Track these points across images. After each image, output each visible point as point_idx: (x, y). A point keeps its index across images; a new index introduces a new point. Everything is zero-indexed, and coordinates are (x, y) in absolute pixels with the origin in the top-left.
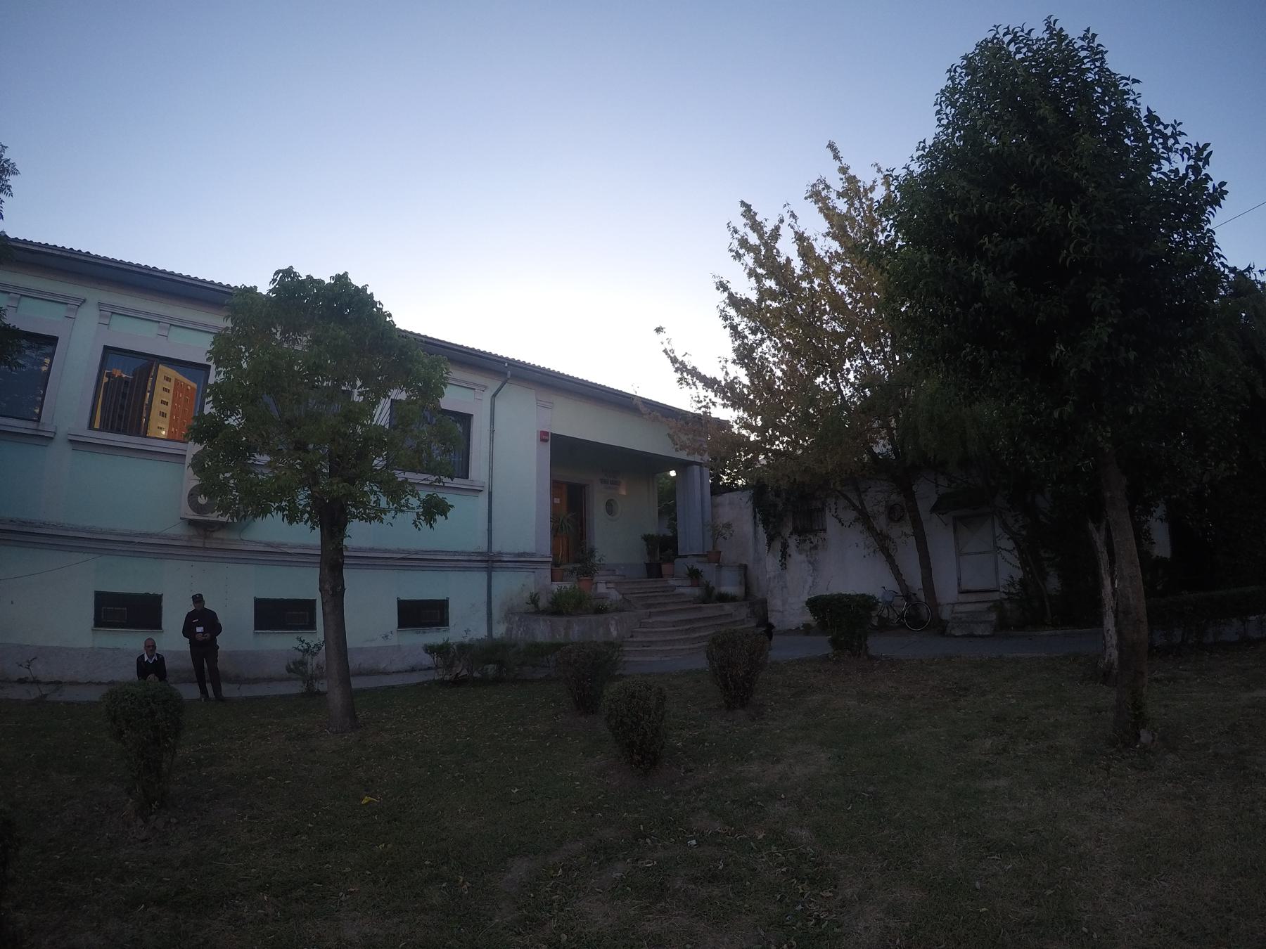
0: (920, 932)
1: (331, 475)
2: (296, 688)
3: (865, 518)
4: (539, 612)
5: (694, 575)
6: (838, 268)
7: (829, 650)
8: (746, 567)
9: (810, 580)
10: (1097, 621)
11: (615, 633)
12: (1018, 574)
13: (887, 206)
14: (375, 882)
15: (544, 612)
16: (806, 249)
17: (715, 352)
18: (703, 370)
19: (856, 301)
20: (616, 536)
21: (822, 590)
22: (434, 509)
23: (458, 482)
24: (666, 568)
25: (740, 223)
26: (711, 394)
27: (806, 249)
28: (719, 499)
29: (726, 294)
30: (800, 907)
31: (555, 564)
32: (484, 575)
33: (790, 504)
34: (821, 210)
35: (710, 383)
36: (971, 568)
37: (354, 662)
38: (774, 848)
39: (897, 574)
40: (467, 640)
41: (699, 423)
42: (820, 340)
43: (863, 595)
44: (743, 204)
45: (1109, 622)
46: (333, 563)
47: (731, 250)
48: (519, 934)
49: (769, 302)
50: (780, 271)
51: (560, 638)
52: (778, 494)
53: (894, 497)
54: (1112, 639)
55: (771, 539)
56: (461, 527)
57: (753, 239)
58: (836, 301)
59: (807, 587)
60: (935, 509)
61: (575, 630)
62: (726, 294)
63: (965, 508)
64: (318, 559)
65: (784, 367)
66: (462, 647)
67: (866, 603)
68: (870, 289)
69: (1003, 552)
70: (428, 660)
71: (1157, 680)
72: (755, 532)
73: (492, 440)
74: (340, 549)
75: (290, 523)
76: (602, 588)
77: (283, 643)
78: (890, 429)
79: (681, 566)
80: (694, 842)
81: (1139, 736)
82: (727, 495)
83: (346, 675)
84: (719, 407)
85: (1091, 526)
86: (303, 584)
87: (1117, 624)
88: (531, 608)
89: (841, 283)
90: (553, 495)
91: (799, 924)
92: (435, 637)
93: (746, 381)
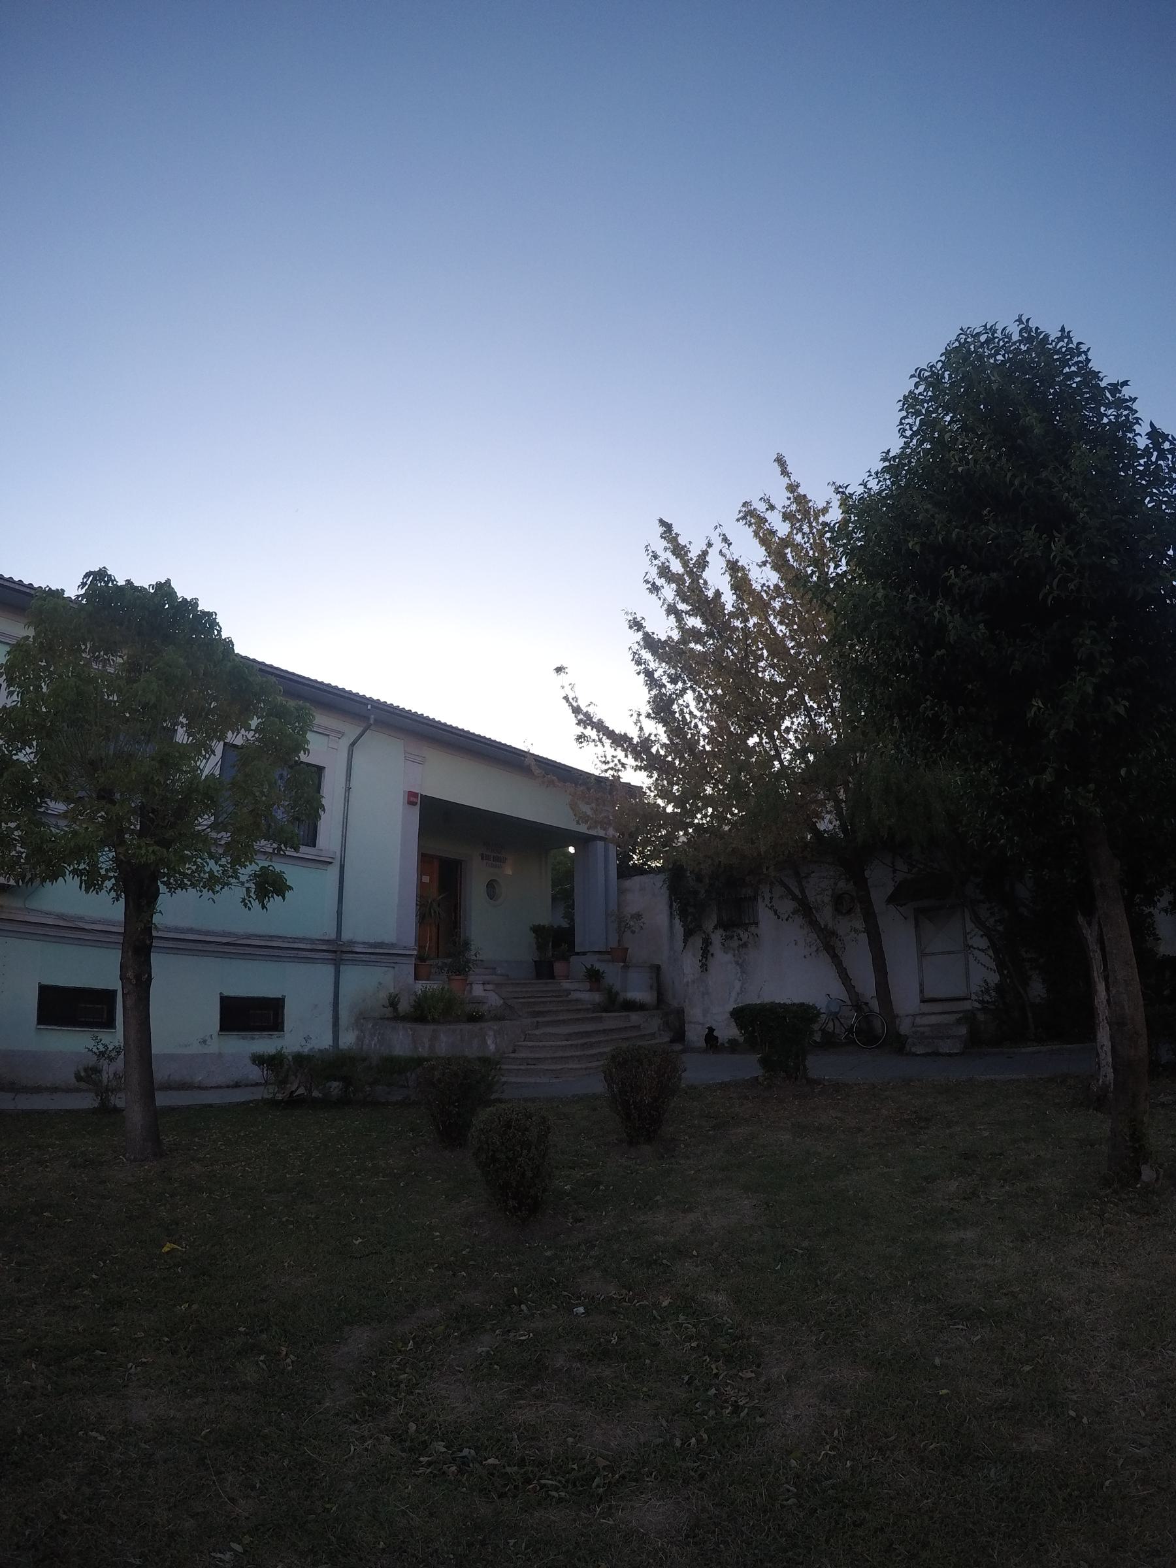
0: (865, 1421)
1: (141, 834)
2: (86, 1101)
3: (806, 910)
4: (397, 1018)
5: (594, 976)
6: (777, 604)
7: (759, 1072)
8: (657, 969)
9: (738, 985)
10: (1089, 1034)
11: (492, 1047)
12: (994, 978)
13: (841, 531)
14: (174, 1353)
15: (405, 1018)
16: (741, 583)
17: (626, 703)
18: (611, 725)
19: (799, 645)
20: (496, 927)
21: (752, 999)
22: (270, 886)
23: (305, 851)
24: (559, 967)
25: (660, 546)
26: (620, 754)
27: (741, 583)
28: (628, 883)
29: (640, 635)
30: (713, 1391)
31: (421, 958)
32: (331, 969)
33: (715, 893)
34: (756, 534)
35: (619, 740)
36: (936, 972)
37: (161, 1073)
38: (682, 1317)
39: (845, 977)
40: (306, 1050)
41: (604, 789)
42: (755, 693)
43: (802, 1004)
44: (662, 523)
45: (1104, 1036)
46: (138, 945)
47: (647, 582)
48: (356, 1422)
49: (692, 645)
50: (707, 607)
51: (423, 1052)
52: (699, 879)
53: (842, 884)
54: (1107, 1058)
55: (688, 934)
56: (307, 905)
57: (676, 567)
58: (776, 646)
59: (734, 994)
60: (893, 899)
61: (444, 1041)
62: (641, 633)
63: (926, 898)
64: (120, 939)
65: (713, 723)
66: (300, 1059)
67: (805, 1014)
68: (816, 631)
69: (976, 952)
70: (256, 1073)
71: (1163, 1105)
72: (671, 926)
73: (347, 800)
74: (148, 928)
75: (87, 891)
76: (478, 991)
77: (73, 1044)
78: (838, 802)
79: (578, 965)
80: (581, 1310)
81: (1140, 1173)
82: (637, 879)
83: (149, 1088)
84: (630, 771)
85: (1080, 919)
86: (100, 970)
87: (1112, 1038)
88: (388, 1012)
89: (781, 623)
90: (422, 871)
91: (712, 1413)
92: (266, 1045)
93: (664, 739)
